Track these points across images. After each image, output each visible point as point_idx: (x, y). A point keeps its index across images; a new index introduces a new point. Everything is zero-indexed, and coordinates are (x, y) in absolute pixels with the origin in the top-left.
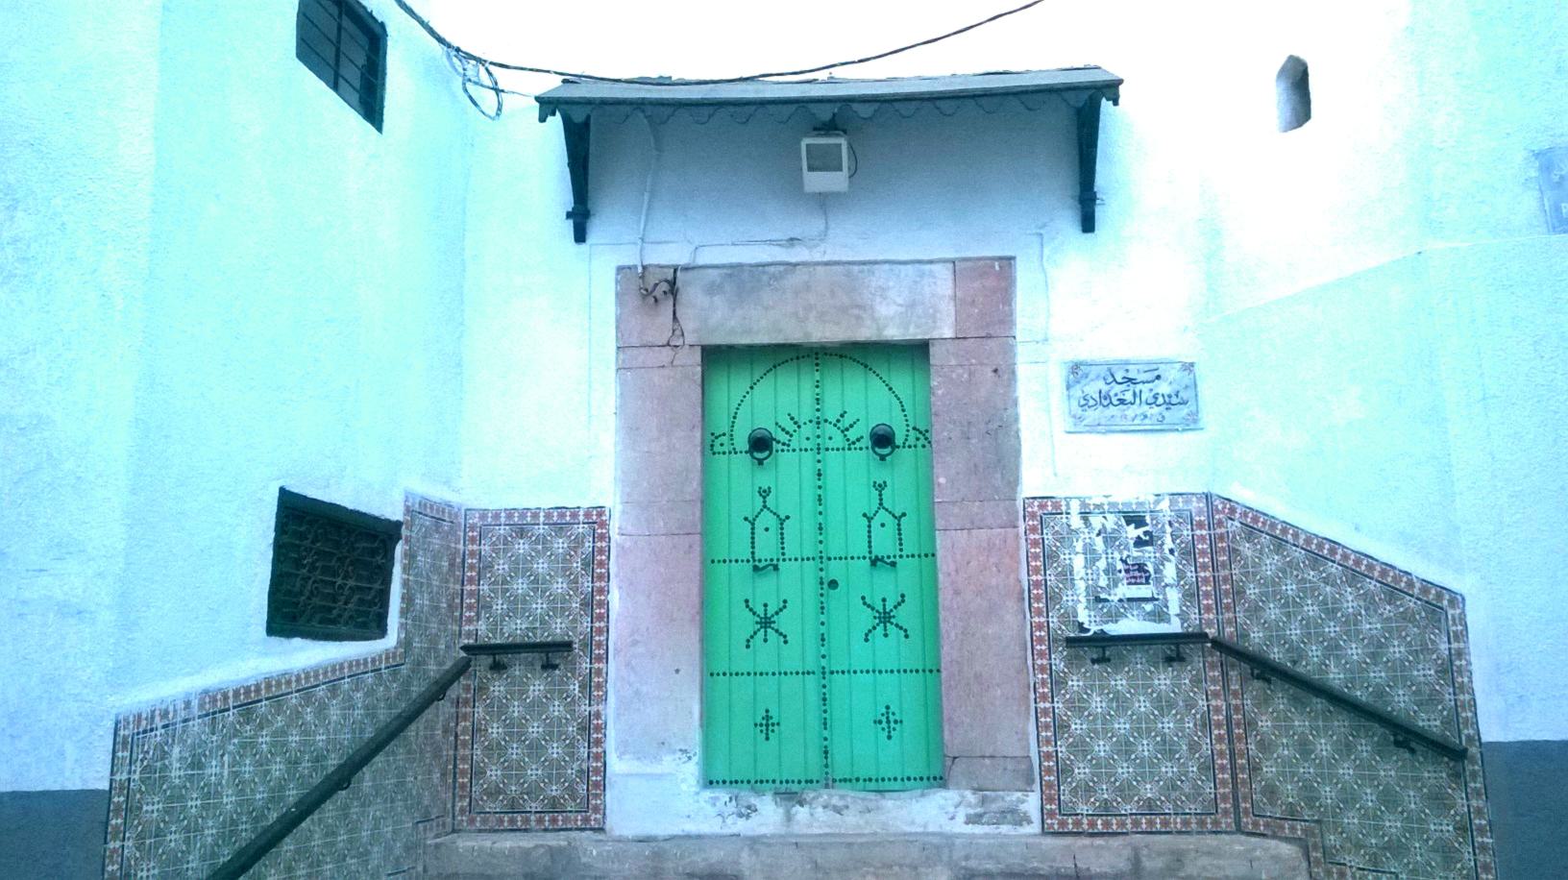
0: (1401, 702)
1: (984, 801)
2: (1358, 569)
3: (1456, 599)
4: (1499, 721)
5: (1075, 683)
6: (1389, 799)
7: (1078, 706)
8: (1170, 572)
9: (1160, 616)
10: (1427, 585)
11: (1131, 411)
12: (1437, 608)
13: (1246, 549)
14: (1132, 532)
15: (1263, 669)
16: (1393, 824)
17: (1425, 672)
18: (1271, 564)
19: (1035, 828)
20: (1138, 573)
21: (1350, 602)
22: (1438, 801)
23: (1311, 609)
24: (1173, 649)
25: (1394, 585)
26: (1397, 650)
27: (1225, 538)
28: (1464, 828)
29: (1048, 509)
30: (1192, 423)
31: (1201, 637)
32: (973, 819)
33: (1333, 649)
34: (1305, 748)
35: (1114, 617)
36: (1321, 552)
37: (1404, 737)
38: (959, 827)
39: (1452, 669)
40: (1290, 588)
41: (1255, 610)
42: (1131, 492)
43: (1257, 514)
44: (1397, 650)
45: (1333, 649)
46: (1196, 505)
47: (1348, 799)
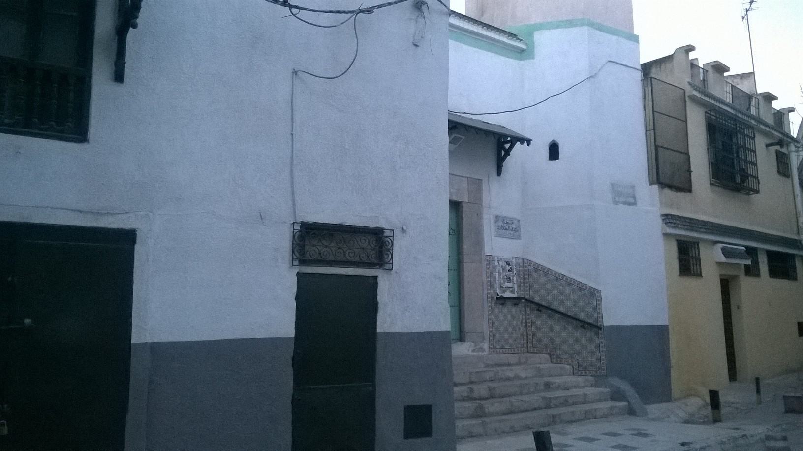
0: (582, 316)
1: (476, 345)
2: (570, 282)
3: (599, 291)
4: (608, 321)
5: (496, 310)
6: (577, 341)
7: (497, 316)
8: (515, 279)
9: (513, 292)
10: (591, 288)
11: (509, 232)
12: (594, 294)
13: (535, 275)
14: (508, 268)
15: (540, 307)
16: (577, 347)
17: (589, 309)
18: (543, 279)
19: (485, 353)
20: (509, 279)
21: (568, 290)
22: (591, 340)
23: (555, 292)
24: (516, 301)
25: (581, 287)
26: (581, 304)
27: (528, 270)
28: (598, 346)
29: (490, 259)
30: (519, 238)
31: (524, 298)
32: (473, 351)
33: (562, 302)
34: (551, 329)
35: (504, 292)
36: (558, 277)
37: (584, 325)
38: (470, 353)
39: (597, 308)
40: (549, 286)
41: (537, 292)
42: (507, 255)
43: (539, 265)
44: (581, 304)
45: (562, 302)
46: (520, 261)
47: (565, 341)
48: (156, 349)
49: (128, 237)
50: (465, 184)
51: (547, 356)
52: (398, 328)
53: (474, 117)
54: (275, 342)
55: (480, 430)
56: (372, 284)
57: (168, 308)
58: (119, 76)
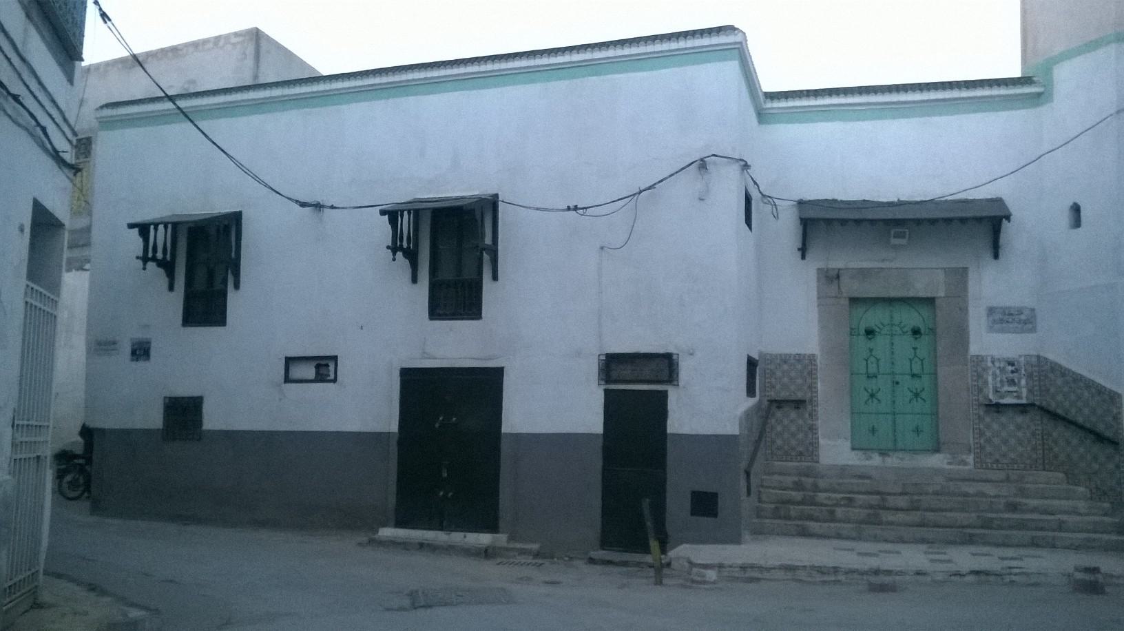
3: (1119, 396)
6: (1095, 458)
8: (1023, 382)
9: (1019, 397)
10: (1111, 391)
13: (1051, 375)
15: (1055, 416)
18: (1059, 382)
19: (971, 467)
20: (1012, 382)
24: (1022, 409)
25: (1100, 390)
27: (1043, 370)
29: (979, 360)
36: (1078, 378)
46: (1034, 360)
48: (518, 437)
49: (499, 373)
50: (941, 276)
51: (1061, 475)
52: (686, 430)
53: (950, 198)
54: (589, 437)
55: (854, 534)
56: (664, 395)
57: (521, 414)
58: (495, 277)
